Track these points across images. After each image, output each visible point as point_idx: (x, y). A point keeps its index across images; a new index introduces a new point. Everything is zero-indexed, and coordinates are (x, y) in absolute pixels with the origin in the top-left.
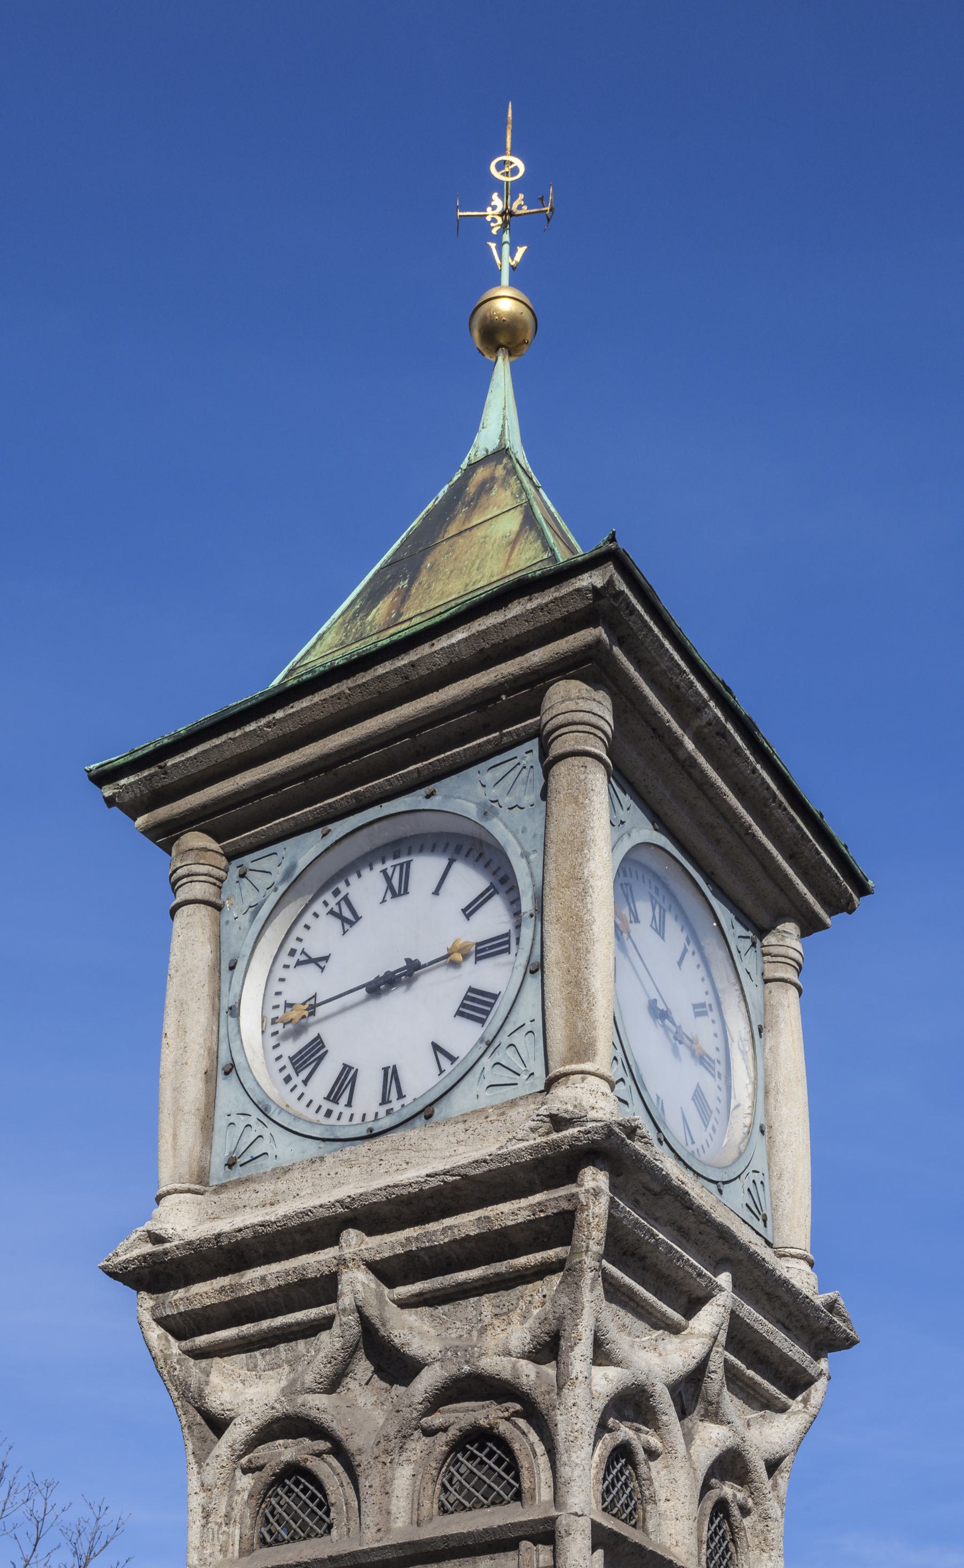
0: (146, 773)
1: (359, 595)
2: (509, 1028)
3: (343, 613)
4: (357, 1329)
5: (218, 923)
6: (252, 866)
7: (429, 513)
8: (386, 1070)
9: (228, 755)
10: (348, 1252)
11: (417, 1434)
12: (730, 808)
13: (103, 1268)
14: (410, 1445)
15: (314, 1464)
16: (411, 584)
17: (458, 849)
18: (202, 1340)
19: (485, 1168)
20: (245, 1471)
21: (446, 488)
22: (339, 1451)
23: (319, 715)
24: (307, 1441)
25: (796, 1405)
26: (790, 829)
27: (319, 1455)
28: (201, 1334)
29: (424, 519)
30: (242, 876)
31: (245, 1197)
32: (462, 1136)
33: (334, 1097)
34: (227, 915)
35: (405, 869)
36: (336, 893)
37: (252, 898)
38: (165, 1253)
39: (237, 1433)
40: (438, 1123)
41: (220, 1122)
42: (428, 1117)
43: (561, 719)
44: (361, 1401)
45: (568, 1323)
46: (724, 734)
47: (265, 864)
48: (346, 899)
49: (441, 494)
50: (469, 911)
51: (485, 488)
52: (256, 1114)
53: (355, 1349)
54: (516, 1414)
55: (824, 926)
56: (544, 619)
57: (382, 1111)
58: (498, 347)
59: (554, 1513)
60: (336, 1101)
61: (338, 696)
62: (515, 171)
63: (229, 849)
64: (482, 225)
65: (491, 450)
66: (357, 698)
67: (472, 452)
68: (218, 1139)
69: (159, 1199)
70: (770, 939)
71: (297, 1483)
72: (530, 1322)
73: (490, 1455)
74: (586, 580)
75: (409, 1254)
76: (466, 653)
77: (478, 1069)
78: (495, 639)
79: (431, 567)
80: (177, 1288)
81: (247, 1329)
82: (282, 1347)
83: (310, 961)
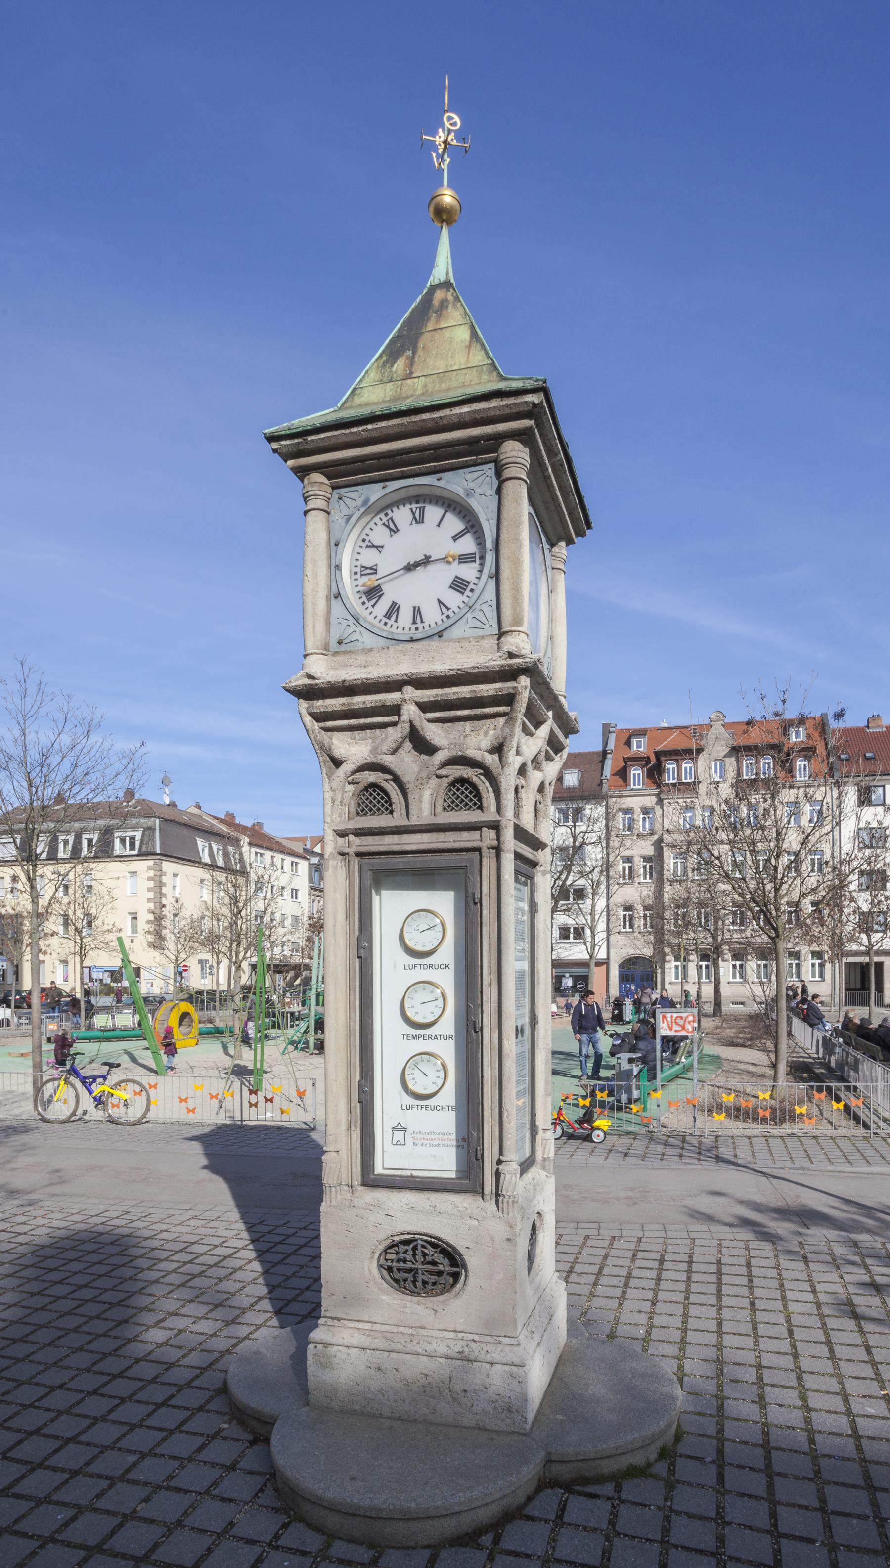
0: (296, 441)
1: (383, 352)
2: (480, 602)
3: (377, 360)
4: (408, 730)
5: (328, 521)
6: (345, 494)
7: (414, 310)
8: (414, 608)
9: (340, 440)
10: (407, 696)
11: (434, 777)
12: (557, 496)
13: (283, 687)
14: (431, 781)
15: (384, 785)
16: (414, 353)
17: (449, 506)
18: (330, 724)
19: (477, 670)
20: (349, 783)
21: (420, 297)
22: (397, 779)
23: (390, 431)
24: (380, 774)
25: (557, 758)
26: (573, 504)
27: (386, 780)
28: (328, 721)
29: (411, 313)
30: (340, 499)
31: (351, 661)
32: (460, 650)
33: (388, 615)
34: (332, 518)
35: (422, 510)
36: (386, 515)
37: (346, 511)
38: (316, 685)
39: (347, 768)
40: (446, 641)
41: (334, 622)
42: (440, 637)
43: (510, 460)
44: (406, 759)
45: (508, 740)
46: (562, 465)
47: (352, 495)
48: (391, 519)
49: (418, 300)
50: (455, 538)
51: (444, 304)
52: (352, 620)
53: (406, 737)
54: (481, 774)
55: (574, 543)
56: (508, 411)
57: (413, 627)
58: (442, 221)
59: (499, 818)
60: (389, 618)
61: (401, 425)
62: (450, 118)
63: (334, 485)
64: (433, 146)
65: (442, 281)
66: (411, 428)
67: (431, 278)
68: (332, 629)
69: (305, 656)
70: (555, 549)
71: (374, 791)
72: (489, 738)
73: (466, 789)
74: (529, 398)
75: (436, 701)
76: (467, 419)
77: (464, 618)
78: (482, 415)
79: (424, 347)
80: (318, 699)
81: (353, 722)
82: (368, 731)
83: (373, 546)
